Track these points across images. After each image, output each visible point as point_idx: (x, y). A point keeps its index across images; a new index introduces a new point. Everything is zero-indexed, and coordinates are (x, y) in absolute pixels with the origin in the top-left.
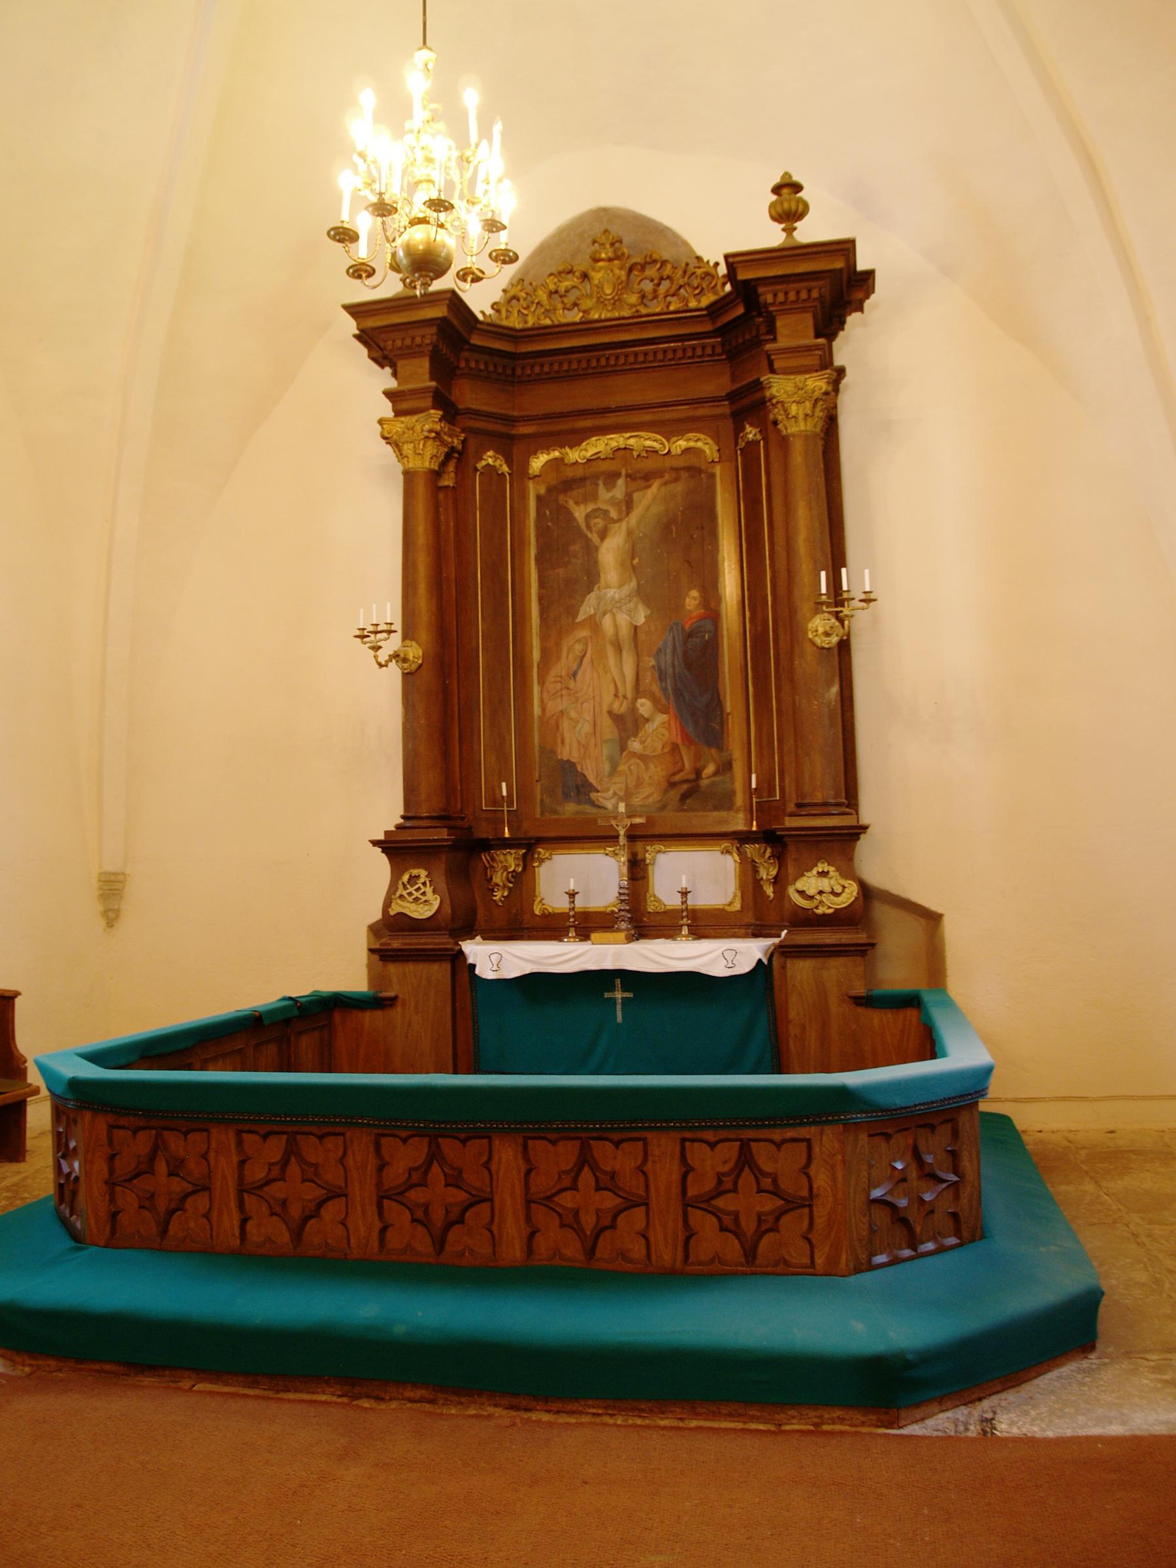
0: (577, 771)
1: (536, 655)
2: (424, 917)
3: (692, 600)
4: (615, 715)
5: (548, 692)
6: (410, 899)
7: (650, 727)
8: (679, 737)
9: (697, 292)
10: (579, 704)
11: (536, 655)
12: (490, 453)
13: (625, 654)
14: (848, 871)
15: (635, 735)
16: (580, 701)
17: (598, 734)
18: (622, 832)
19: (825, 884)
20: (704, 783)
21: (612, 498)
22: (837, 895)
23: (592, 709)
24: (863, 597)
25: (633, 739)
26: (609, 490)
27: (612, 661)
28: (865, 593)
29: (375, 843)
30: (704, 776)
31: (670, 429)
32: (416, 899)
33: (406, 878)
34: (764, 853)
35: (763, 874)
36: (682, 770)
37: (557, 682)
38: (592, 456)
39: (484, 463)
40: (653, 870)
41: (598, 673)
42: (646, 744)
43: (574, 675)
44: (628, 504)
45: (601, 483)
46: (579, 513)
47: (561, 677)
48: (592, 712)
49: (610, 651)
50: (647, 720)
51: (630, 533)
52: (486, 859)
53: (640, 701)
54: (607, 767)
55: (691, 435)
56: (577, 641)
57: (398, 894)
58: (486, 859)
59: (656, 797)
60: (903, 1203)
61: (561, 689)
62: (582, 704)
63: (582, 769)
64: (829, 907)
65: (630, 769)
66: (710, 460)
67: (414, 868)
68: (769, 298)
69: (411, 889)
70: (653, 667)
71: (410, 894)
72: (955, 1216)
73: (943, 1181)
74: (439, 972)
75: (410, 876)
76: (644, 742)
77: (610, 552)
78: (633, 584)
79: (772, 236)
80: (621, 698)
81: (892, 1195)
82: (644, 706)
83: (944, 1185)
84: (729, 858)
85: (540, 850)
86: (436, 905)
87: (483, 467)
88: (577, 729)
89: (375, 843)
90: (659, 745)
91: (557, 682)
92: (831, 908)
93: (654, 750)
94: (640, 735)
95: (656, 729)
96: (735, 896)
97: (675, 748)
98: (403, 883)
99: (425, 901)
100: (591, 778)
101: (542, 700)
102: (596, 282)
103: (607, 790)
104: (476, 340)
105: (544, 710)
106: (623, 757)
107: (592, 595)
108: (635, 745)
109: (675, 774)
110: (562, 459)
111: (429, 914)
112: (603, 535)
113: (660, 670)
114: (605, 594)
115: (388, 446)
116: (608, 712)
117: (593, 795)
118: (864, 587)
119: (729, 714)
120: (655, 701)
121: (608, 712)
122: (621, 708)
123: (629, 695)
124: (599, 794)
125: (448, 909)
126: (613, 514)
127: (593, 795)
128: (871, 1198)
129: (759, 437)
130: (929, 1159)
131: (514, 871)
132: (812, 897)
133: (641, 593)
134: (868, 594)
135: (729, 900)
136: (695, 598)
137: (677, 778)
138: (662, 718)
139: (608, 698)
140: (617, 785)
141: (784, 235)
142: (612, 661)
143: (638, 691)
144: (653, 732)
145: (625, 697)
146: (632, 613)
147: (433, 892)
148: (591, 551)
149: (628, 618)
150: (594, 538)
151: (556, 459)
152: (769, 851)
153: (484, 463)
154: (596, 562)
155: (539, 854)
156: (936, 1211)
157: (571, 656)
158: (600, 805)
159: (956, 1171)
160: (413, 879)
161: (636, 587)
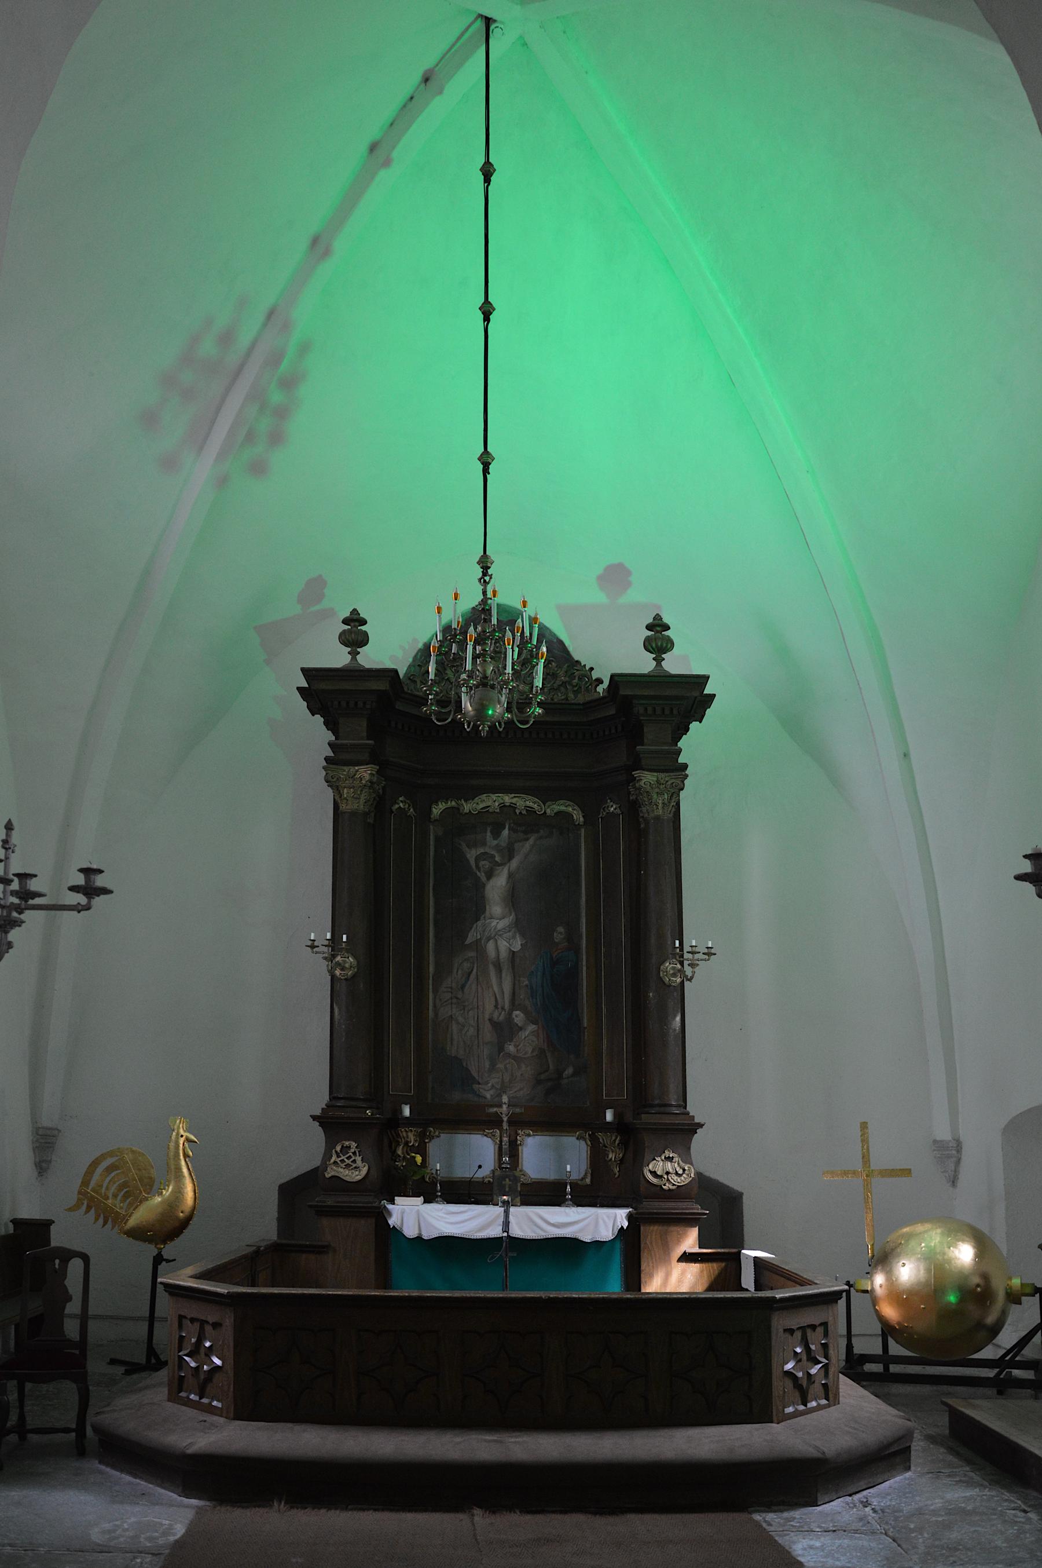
0: (463, 1067)
2: (355, 1181)
3: (559, 934)
4: (495, 1022)
5: (440, 1000)
6: (343, 1165)
7: (523, 1035)
8: (546, 1044)
9: (576, 689)
10: (466, 1012)
13: (504, 975)
14: (687, 1158)
15: (511, 1040)
16: (466, 1009)
17: (480, 1036)
18: (505, 1119)
19: (669, 1166)
20: (564, 1082)
21: (497, 845)
23: (476, 1016)
24: (706, 951)
25: (509, 1043)
26: (495, 839)
28: (707, 948)
29: (314, 1118)
30: (564, 1076)
31: (546, 795)
33: (338, 1148)
34: (615, 1140)
35: (611, 1156)
36: (547, 1071)
37: (449, 992)
38: (481, 809)
39: (397, 806)
40: (522, 1150)
41: (483, 989)
42: (519, 1048)
43: (463, 987)
44: (509, 853)
45: (489, 829)
46: (471, 855)
47: (451, 988)
48: (476, 1018)
49: (491, 968)
50: (521, 1029)
51: (511, 875)
52: (392, 1134)
54: (487, 1064)
55: (562, 802)
56: (465, 960)
58: (392, 1134)
60: (800, 1374)
61: (451, 998)
62: (468, 1013)
63: (467, 1064)
64: (674, 1185)
65: (506, 1068)
66: (577, 823)
68: (641, 710)
70: (527, 986)
71: (342, 1161)
72: (825, 1386)
74: (365, 1226)
75: (342, 1146)
76: (518, 1046)
77: (497, 886)
78: (512, 917)
79: (644, 663)
80: (500, 1010)
81: (794, 1370)
82: (518, 1017)
83: (821, 1365)
84: (583, 1143)
87: (396, 809)
88: (464, 1032)
89: (314, 1118)
91: (449, 992)
92: (675, 1185)
93: (526, 1053)
94: (514, 1040)
95: (527, 1036)
97: (542, 1052)
98: (336, 1152)
99: (355, 1168)
100: (475, 1074)
101: (435, 1006)
103: (487, 1083)
104: (399, 706)
105: (436, 1015)
106: (500, 1056)
107: (479, 923)
108: (511, 1048)
110: (458, 809)
111: (359, 1178)
112: (490, 875)
114: (490, 923)
115: (330, 788)
116: (489, 1020)
117: (476, 1087)
118: (708, 944)
119: (585, 1028)
121: (489, 1020)
123: (507, 1006)
124: (480, 1086)
126: (497, 859)
127: (476, 1087)
128: (785, 1370)
129: (618, 811)
130: (813, 1347)
131: (413, 1145)
132: (661, 1177)
134: (710, 949)
135: (582, 1175)
136: (561, 933)
137: (543, 1077)
138: (532, 1027)
139: (489, 1007)
140: (494, 1080)
141: (654, 663)
143: (514, 1005)
144: (525, 1038)
145: (503, 1008)
146: (511, 941)
147: (362, 1160)
148: (479, 888)
149: (508, 945)
150: (484, 879)
151: (452, 808)
153: (397, 806)
154: (483, 897)
155: (430, 1132)
156: (816, 1382)
157: (460, 972)
158: (481, 1095)
159: (826, 1357)
160: (345, 1149)
161: (514, 920)
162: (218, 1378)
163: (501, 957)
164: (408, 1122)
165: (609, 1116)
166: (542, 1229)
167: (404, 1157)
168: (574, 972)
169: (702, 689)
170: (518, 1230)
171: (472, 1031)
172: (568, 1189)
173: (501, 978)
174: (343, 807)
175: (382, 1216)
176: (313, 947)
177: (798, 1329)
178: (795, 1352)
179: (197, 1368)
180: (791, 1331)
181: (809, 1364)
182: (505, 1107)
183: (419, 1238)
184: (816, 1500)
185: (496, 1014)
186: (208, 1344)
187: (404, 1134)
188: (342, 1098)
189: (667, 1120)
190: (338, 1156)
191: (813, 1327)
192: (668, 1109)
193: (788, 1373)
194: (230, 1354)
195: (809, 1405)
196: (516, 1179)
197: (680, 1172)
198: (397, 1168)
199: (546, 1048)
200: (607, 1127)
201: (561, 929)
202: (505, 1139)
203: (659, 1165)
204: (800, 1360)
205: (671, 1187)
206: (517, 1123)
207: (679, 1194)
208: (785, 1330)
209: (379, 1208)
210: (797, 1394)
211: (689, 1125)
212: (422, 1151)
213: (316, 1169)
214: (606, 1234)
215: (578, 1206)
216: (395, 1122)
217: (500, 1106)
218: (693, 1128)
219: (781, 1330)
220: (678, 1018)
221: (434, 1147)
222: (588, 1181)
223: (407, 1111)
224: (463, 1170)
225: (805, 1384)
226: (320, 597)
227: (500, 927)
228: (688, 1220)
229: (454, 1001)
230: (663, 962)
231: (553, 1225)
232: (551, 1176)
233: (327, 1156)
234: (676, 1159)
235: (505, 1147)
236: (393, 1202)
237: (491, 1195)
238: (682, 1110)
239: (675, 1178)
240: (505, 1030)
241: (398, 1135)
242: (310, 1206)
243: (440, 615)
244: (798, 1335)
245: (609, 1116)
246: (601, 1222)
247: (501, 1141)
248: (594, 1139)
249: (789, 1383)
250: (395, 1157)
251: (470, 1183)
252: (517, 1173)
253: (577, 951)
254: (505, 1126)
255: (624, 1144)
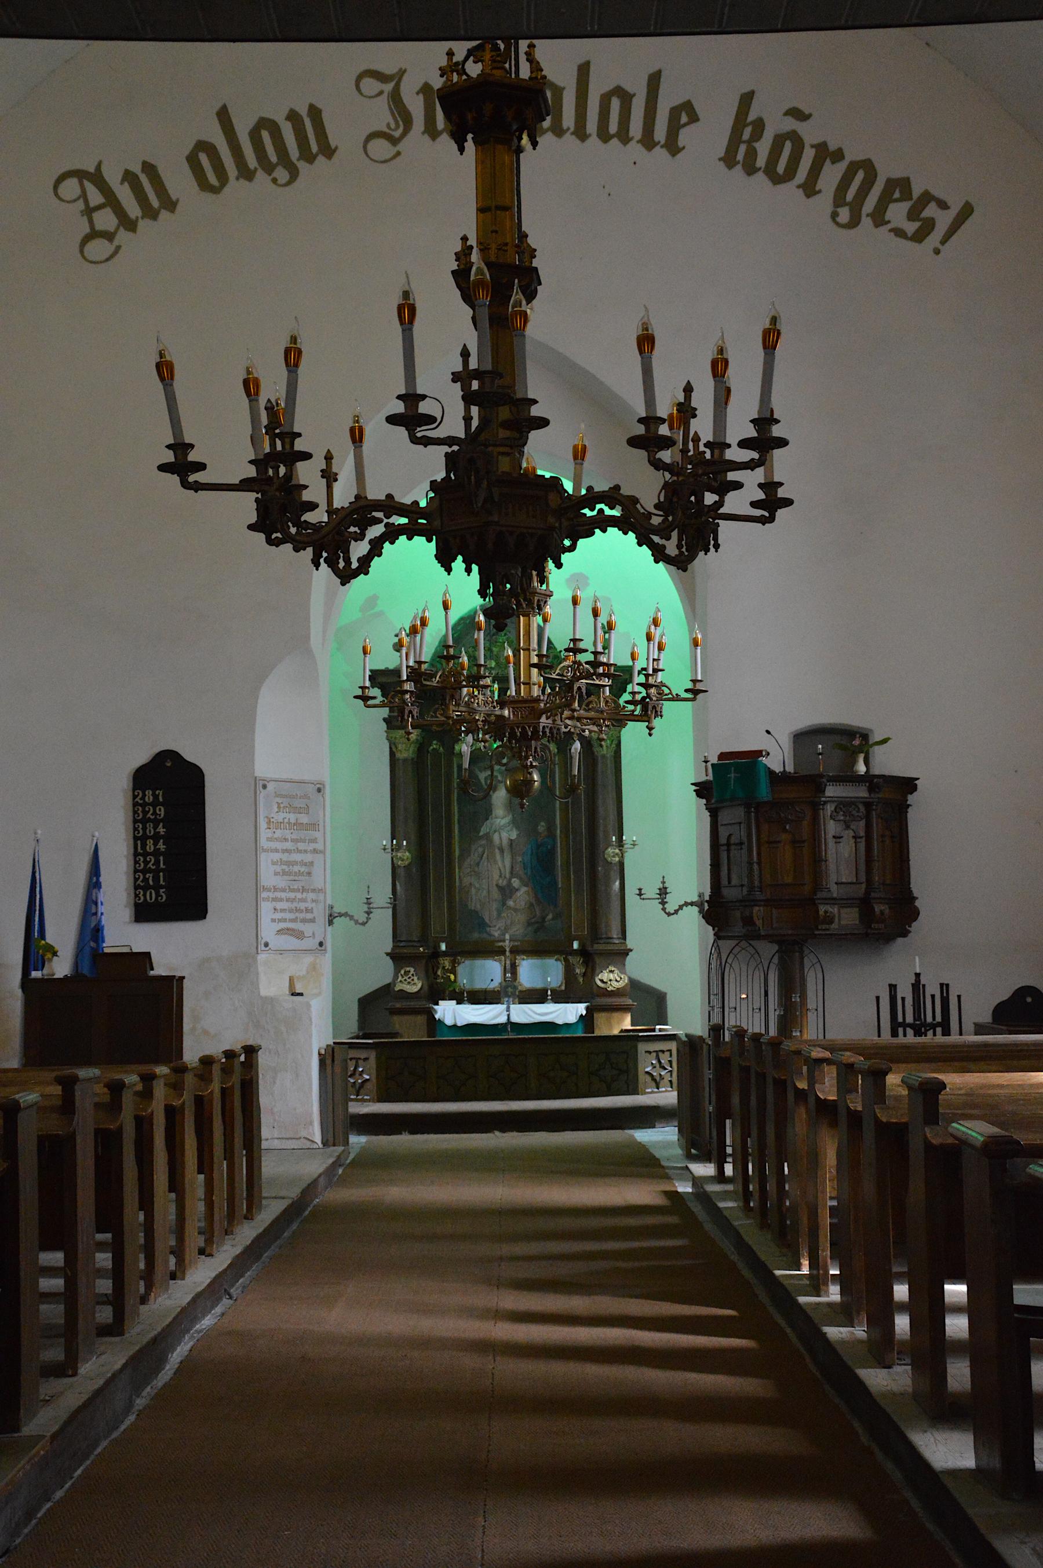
1: (457, 853)
3: (542, 827)
6: (406, 983)
7: (518, 894)
11: (457, 853)
12: (435, 742)
13: (505, 854)
14: (623, 971)
15: (511, 897)
18: (508, 950)
19: (611, 976)
22: (618, 982)
24: (632, 843)
27: (498, 857)
29: (387, 954)
32: (409, 983)
33: (402, 972)
35: (578, 971)
39: (432, 748)
43: (478, 864)
49: (497, 850)
50: (517, 890)
53: (513, 880)
54: (495, 913)
57: (399, 980)
59: (522, 931)
60: (655, 1074)
67: (407, 967)
69: (405, 978)
73: (666, 1069)
74: (421, 1019)
78: (511, 816)
82: (516, 883)
84: (559, 963)
85: (459, 958)
86: (419, 985)
90: (523, 903)
96: (562, 983)
97: (532, 905)
101: (460, 877)
102: (495, 653)
103: (495, 926)
108: (511, 903)
109: (531, 919)
111: (416, 990)
113: (524, 864)
120: (521, 879)
122: (503, 883)
123: (508, 876)
125: (426, 988)
130: (663, 1061)
132: (606, 983)
133: (514, 822)
136: (543, 826)
137: (533, 920)
138: (524, 889)
139: (496, 876)
140: (501, 924)
142: (498, 857)
145: (505, 877)
152: (582, 960)
153: (432, 748)
157: (476, 855)
159: (671, 1067)
160: (407, 973)
162: (368, 1086)
163: (503, 845)
164: (445, 954)
165: (576, 945)
166: (531, 1016)
167: (442, 977)
168: (552, 852)
169: (491, 1001)
170: (516, 1018)
171: (485, 893)
172: (549, 993)
173: (503, 857)
174: (398, 755)
175: (430, 1014)
176: (385, 849)
177: (654, 1051)
178: (652, 1063)
179: (354, 1083)
180: (650, 1052)
181: (661, 1069)
182: (507, 942)
183: (455, 1026)
184: (655, 1125)
185: (501, 881)
186: (361, 1069)
187: (442, 962)
188: (404, 941)
189: (610, 947)
190: (403, 977)
191: (663, 1052)
192: (611, 941)
193: (647, 1073)
194: (374, 1072)
195: (660, 1090)
196: (515, 988)
197: (619, 979)
198: (437, 983)
199: (534, 902)
200: (574, 953)
201: (543, 824)
202: (508, 962)
203: (605, 975)
204: (655, 1067)
205: (613, 989)
206: (515, 951)
207: (618, 993)
208: (646, 1052)
209: (430, 1008)
210: (654, 1084)
211: (624, 950)
212: (453, 971)
213: (389, 985)
214: (572, 1019)
215: (555, 1003)
216: (436, 954)
217: (504, 941)
218: (626, 952)
219: (643, 1052)
220: (617, 883)
221: (460, 969)
222: (563, 988)
223: (443, 947)
224: (480, 985)
225: (658, 1079)
226: (375, 605)
227: (502, 824)
228: (623, 1009)
229: (473, 873)
230: (607, 848)
231: (539, 1014)
232: (539, 985)
233: (396, 977)
234: (616, 971)
235: (508, 967)
236: (437, 1004)
237: (500, 999)
238: (623, 941)
239: (616, 983)
240: (506, 892)
241: (439, 963)
242: (386, 1009)
243: (407, 288)
244: (654, 1054)
245: (576, 945)
246: (568, 1012)
247: (505, 964)
248: (566, 960)
249: (648, 1078)
250: (436, 977)
251: (485, 992)
252: (516, 984)
253: (554, 837)
254: (508, 954)
255: (586, 963)
